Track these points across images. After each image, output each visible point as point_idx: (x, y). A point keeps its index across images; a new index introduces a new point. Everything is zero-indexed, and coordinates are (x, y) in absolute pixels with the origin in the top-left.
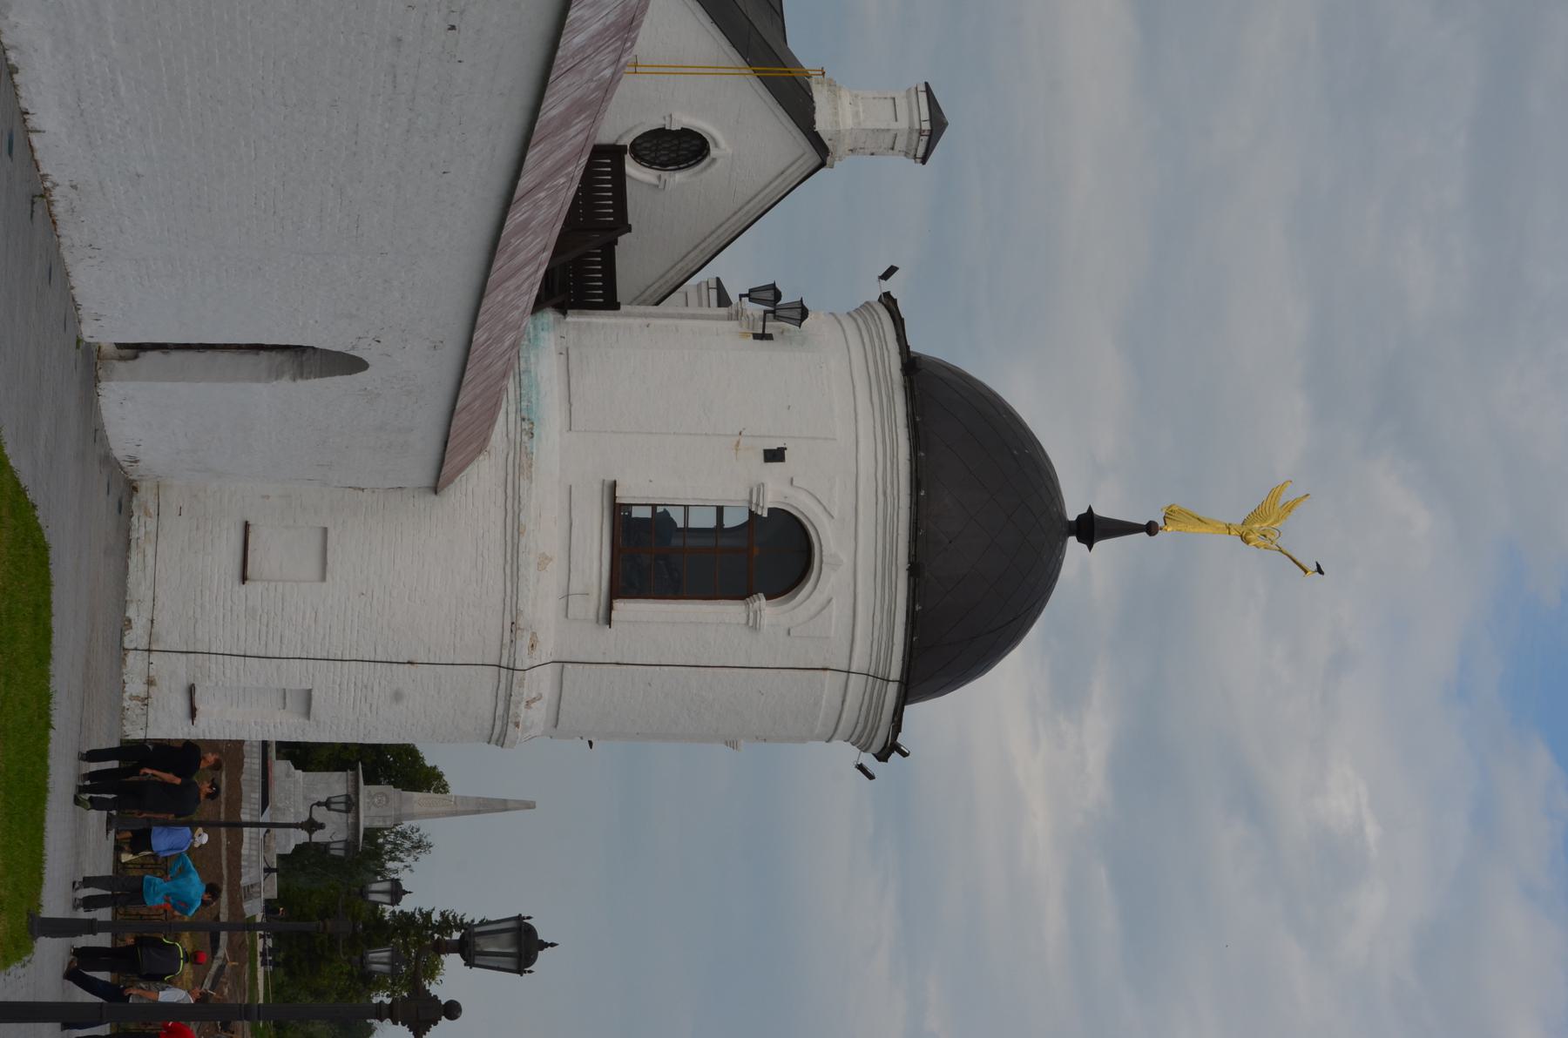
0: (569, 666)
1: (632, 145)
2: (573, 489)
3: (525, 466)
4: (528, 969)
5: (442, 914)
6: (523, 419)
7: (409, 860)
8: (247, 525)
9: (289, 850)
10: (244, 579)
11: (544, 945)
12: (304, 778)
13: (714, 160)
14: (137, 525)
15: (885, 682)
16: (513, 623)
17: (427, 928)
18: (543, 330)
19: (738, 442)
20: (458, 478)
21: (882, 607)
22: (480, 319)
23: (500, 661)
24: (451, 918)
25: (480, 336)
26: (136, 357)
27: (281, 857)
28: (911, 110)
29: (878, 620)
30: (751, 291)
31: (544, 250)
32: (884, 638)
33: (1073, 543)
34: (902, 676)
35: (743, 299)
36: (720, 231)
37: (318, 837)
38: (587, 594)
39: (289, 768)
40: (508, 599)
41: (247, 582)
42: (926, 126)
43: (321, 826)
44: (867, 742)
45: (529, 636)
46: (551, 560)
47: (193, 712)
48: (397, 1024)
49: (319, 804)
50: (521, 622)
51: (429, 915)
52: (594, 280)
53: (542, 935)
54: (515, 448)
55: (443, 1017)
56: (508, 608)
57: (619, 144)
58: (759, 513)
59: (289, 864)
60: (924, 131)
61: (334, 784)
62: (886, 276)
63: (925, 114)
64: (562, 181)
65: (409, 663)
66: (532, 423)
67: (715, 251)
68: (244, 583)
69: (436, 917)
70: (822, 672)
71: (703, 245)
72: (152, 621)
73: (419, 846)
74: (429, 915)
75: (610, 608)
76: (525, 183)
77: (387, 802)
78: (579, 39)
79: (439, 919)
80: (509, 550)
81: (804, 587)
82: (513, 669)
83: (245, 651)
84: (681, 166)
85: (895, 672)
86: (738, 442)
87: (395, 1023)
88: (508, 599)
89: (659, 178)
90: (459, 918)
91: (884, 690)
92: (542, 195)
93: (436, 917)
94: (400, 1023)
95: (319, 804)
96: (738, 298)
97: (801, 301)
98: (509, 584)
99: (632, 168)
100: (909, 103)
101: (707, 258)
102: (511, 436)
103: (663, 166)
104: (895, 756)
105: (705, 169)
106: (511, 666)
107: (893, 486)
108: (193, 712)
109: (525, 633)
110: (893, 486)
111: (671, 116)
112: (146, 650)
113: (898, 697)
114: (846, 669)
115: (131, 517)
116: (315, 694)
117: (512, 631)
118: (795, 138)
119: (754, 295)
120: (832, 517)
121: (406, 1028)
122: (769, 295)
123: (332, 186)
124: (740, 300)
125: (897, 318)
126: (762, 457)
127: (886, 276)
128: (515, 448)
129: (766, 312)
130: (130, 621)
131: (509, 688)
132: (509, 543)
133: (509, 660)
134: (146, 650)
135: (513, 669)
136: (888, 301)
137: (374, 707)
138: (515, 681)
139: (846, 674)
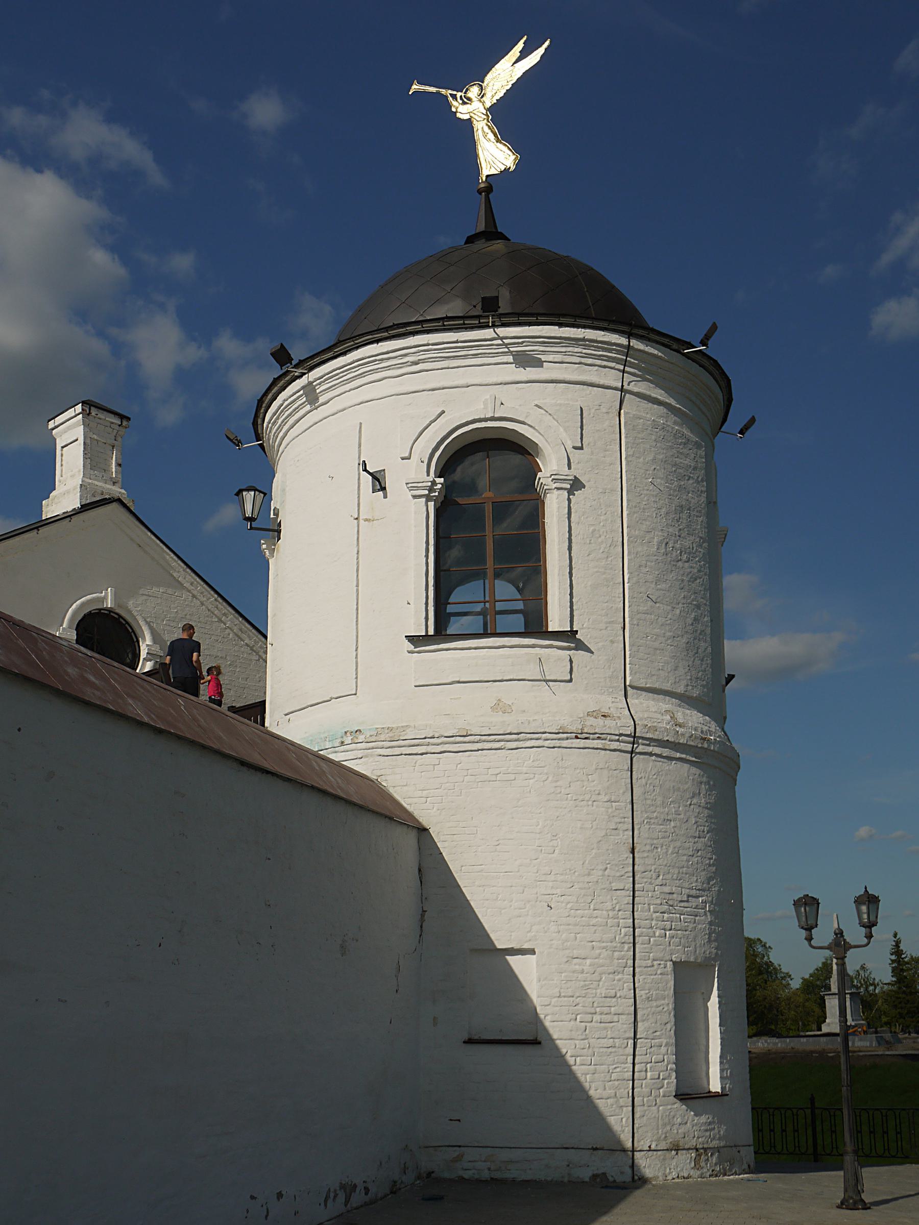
2: (417, 684)
3: (391, 734)
5: (892, 955)
6: (342, 743)
14: (473, 1171)
16: (577, 737)
17: (900, 961)
19: (366, 520)
20: (408, 807)
24: (893, 951)
29: (558, 358)
32: (579, 350)
40: (547, 743)
43: (839, 933)
45: (592, 719)
46: (499, 700)
49: (809, 939)
50: (575, 727)
51: (893, 961)
54: (373, 748)
56: (557, 743)
60: (83, 409)
65: (633, 852)
66: (346, 733)
68: (540, 1043)
69: (893, 957)
73: (863, 968)
74: (893, 961)
79: (894, 956)
86: (366, 520)
88: (547, 743)
93: (893, 957)
95: (809, 939)
98: (529, 743)
100: (65, 431)
102: (359, 754)
107: (406, 355)
109: (588, 723)
110: (406, 355)
115: (463, 1178)
117: (586, 738)
128: (373, 748)
130: (595, 1176)
132: (479, 746)
137: (694, 892)
138: (649, 735)
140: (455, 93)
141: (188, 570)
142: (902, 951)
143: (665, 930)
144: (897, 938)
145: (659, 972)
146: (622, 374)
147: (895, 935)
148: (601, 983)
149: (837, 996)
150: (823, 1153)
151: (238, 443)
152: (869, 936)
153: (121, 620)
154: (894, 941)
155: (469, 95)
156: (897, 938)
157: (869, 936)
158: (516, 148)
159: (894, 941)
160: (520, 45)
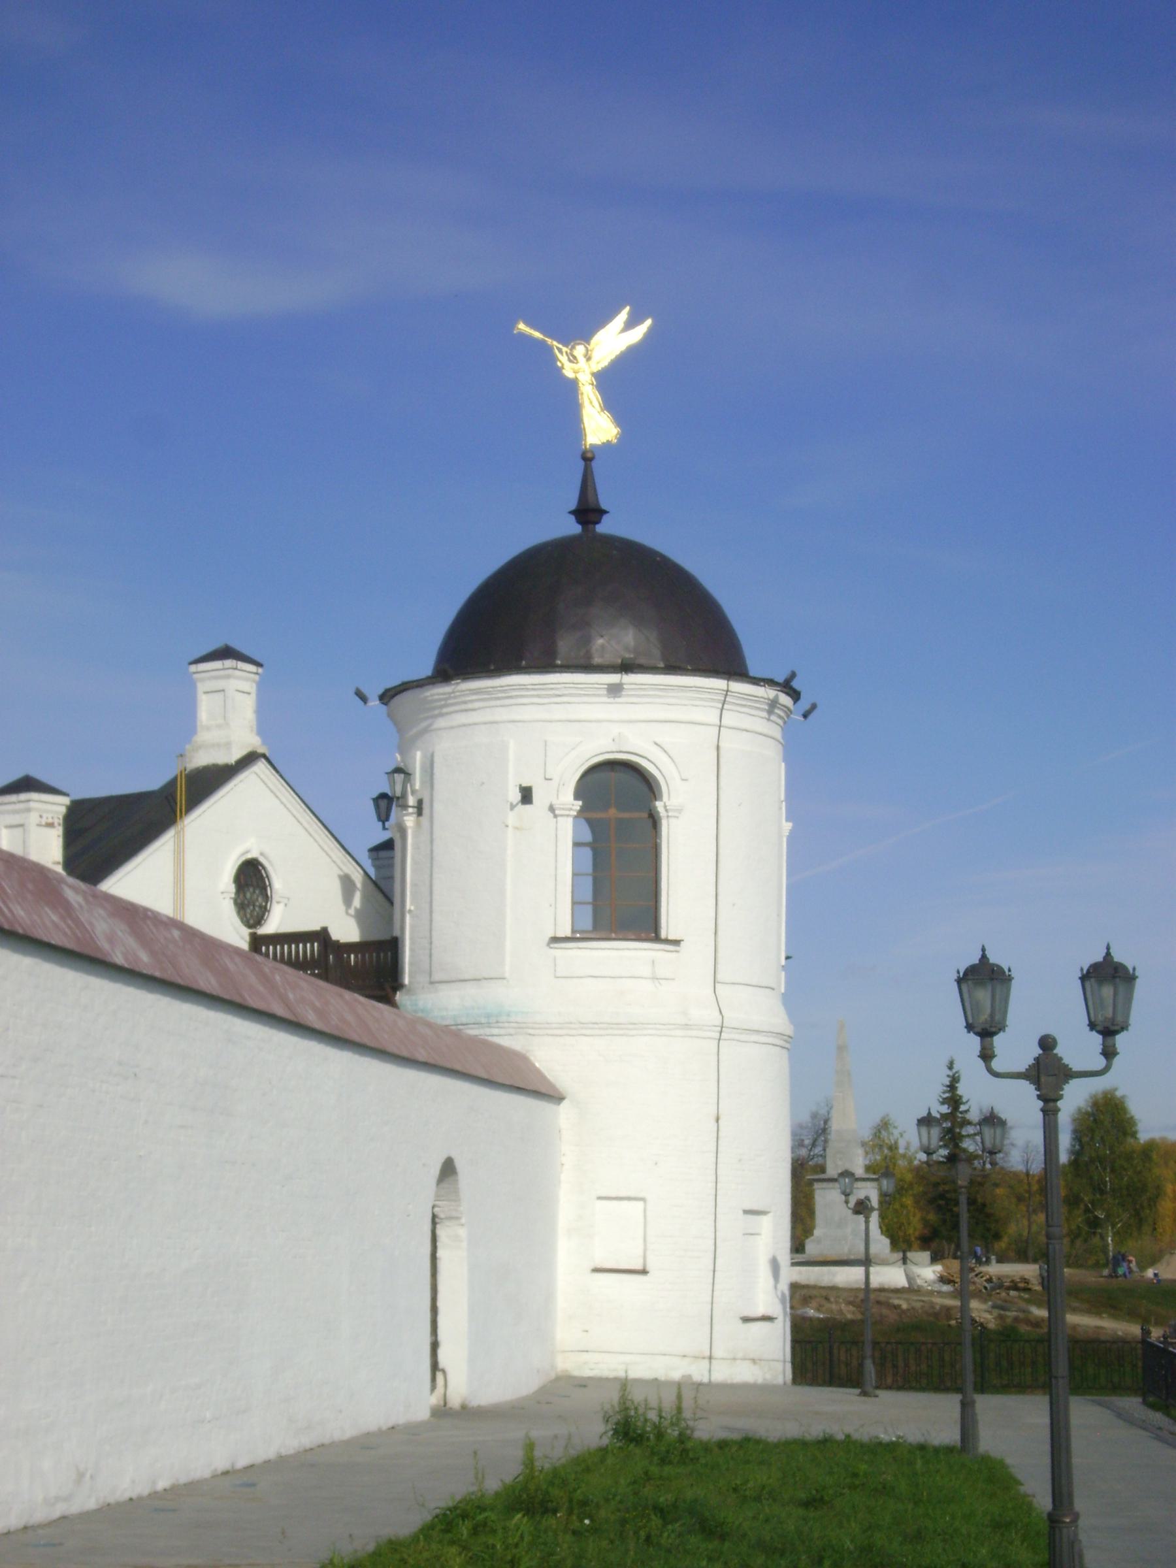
1: (250, 926)
4: (1007, 973)
5: (943, 1103)
7: (896, 1133)
8: (597, 1270)
9: (886, 1242)
10: (644, 1272)
11: (984, 957)
13: (262, 854)
15: (729, 693)
21: (660, 697)
22: (405, 1054)
23: (715, 1039)
25: (422, 1055)
26: (443, 1371)
30: (379, 819)
31: (341, 996)
33: (604, 527)
34: (724, 679)
35: (387, 826)
36: (326, 848)
37: (875, 1202)
38: (653, 962)
43: (1047, 1044)
44: (782, 709)
48: (1062, 1095)
49: (986, 1056)
53: (975, 959)
55: (1055, 1052)
59: (901, 1243)
61: (828, 1200)
62: (363, 698)
64: (278, 978)
67: (344, 852)
72: (684, 1356)
75: (667, 941)
76: (279, 1010)
78: (144, 957)
79: (946, 1106)
80: (616, 1032)
81: (645, 769)
82: (722, 1027)
83: (717, 1032)
84: (267, 883)
85: (719, 683)
87: (1061, 1097)
89: (278, 902)
90: (945, 1088)
91: (736, 694)
92: (291, 996)
94: (1061, 1093)
95: (986, 1056)
96: (386, 831)
97: (387, 773)
99: (270, 927)
100: (211, 678)
101: (350, 859)
103: (267, 898)
104: (795, 684)
105: (270, 862)
106: (719, 1029)
111: (222, 893)
112: (710, 1363)
113: (742, 681)
118: (241, 781)
119: (383, 818)
120: (581, 742)
121: (1066, 1087)
122: (383, 803)
123: (283, 1186)
124: (387, 829)
125: (402, 688)
126: (528, 807)
127: (363, 698)
129: (398, 806)
131: (739, 1031)
133: (714, 1031)
134: (710, 1363)
135: (722, 1027)
136: (387, 697)
140: (560, 346)
142: (961, 1097)
144: (954, 1071)
146: (722, 724)
147: (950, 1067)
152: (1109, 1053)
154: (948, 1076)
155: (575, 353)
156: (954, 1071)
157: (1109, 1053)
158: (618, 420)
159: (948, 1076)
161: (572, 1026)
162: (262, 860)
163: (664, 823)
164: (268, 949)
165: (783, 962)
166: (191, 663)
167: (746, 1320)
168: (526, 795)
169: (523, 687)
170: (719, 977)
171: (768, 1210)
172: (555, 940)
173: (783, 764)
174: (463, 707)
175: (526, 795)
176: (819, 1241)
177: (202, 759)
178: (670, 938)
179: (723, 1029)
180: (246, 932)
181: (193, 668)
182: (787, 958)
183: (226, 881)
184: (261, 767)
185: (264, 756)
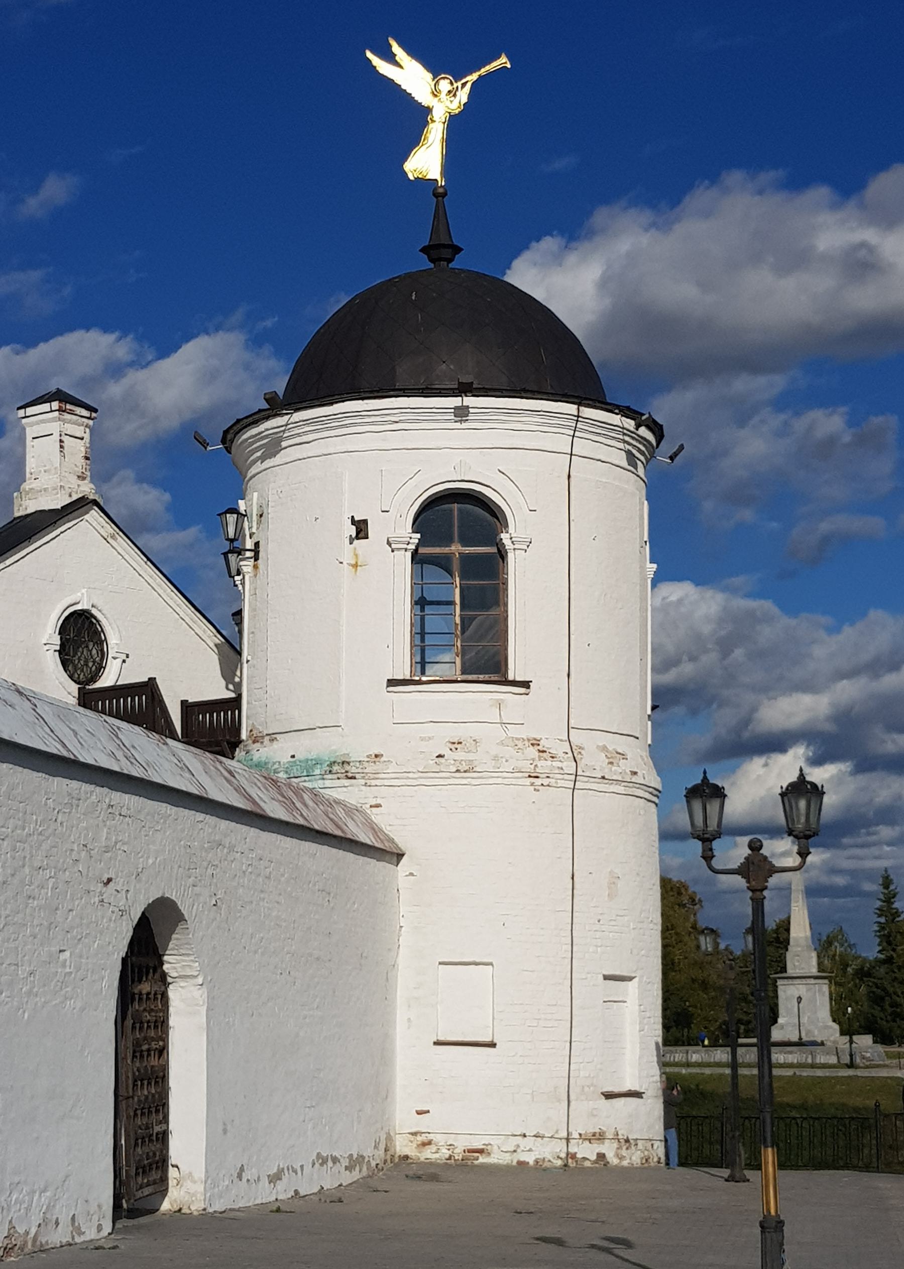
0: (572, 721)
10: (492, 1045)
12: (784, 1017)
18: (252, 760)
27: (842, 1033)
28: (43, 421)
39: (776, 1027)
41: (495, 1041)
42: (55, 405)
47: (637, 1095)
52: (226, 719)
56: (514, 781)
57: (77, 695)
58: (417, 541)
60: (60, 406)
63: (45, 407)
66: (334, 762)
70: (571, 479)
71: (187, 619)
77: (798, 956)
89: (114, 658)
98: (491, 781)
100: (37, 423)
103: (103, 655)
106: (573, 777)
108: (637, 1095)
114: (569, 456)
116: (606, 973)
135: (576, 776)
137: (621, 913)
139: (570, 453)
141: (149, 563)
143: (597, 946)
145: (592, 984)
148: (247, 840)
149: (755, 1049)
150: (73, 1242)
151: (204, 444)
153: (102, 635)
160: (376, 61)
161: (410, 775)
162: (94, 612)
163: (511, 556)
164: (103, 705)
165: (649, 712)
166: (19, 408)
167: (609, 1096)
168: (361, 529)
169: (357, 414)
170: (572, 724)
171: (633, 975)
172: (392, 683)
173: (646, 502)
174: (298, 440)
175: (361, 529)
176: (782, 1027)
177: (27, 506)
178: (518, 679)
179: (578, 777)
180: (74, 688)
181: (21, 413)
182: (654, 708)
183: (50, 635)
184: (94, 515)
185: (95, 503)
